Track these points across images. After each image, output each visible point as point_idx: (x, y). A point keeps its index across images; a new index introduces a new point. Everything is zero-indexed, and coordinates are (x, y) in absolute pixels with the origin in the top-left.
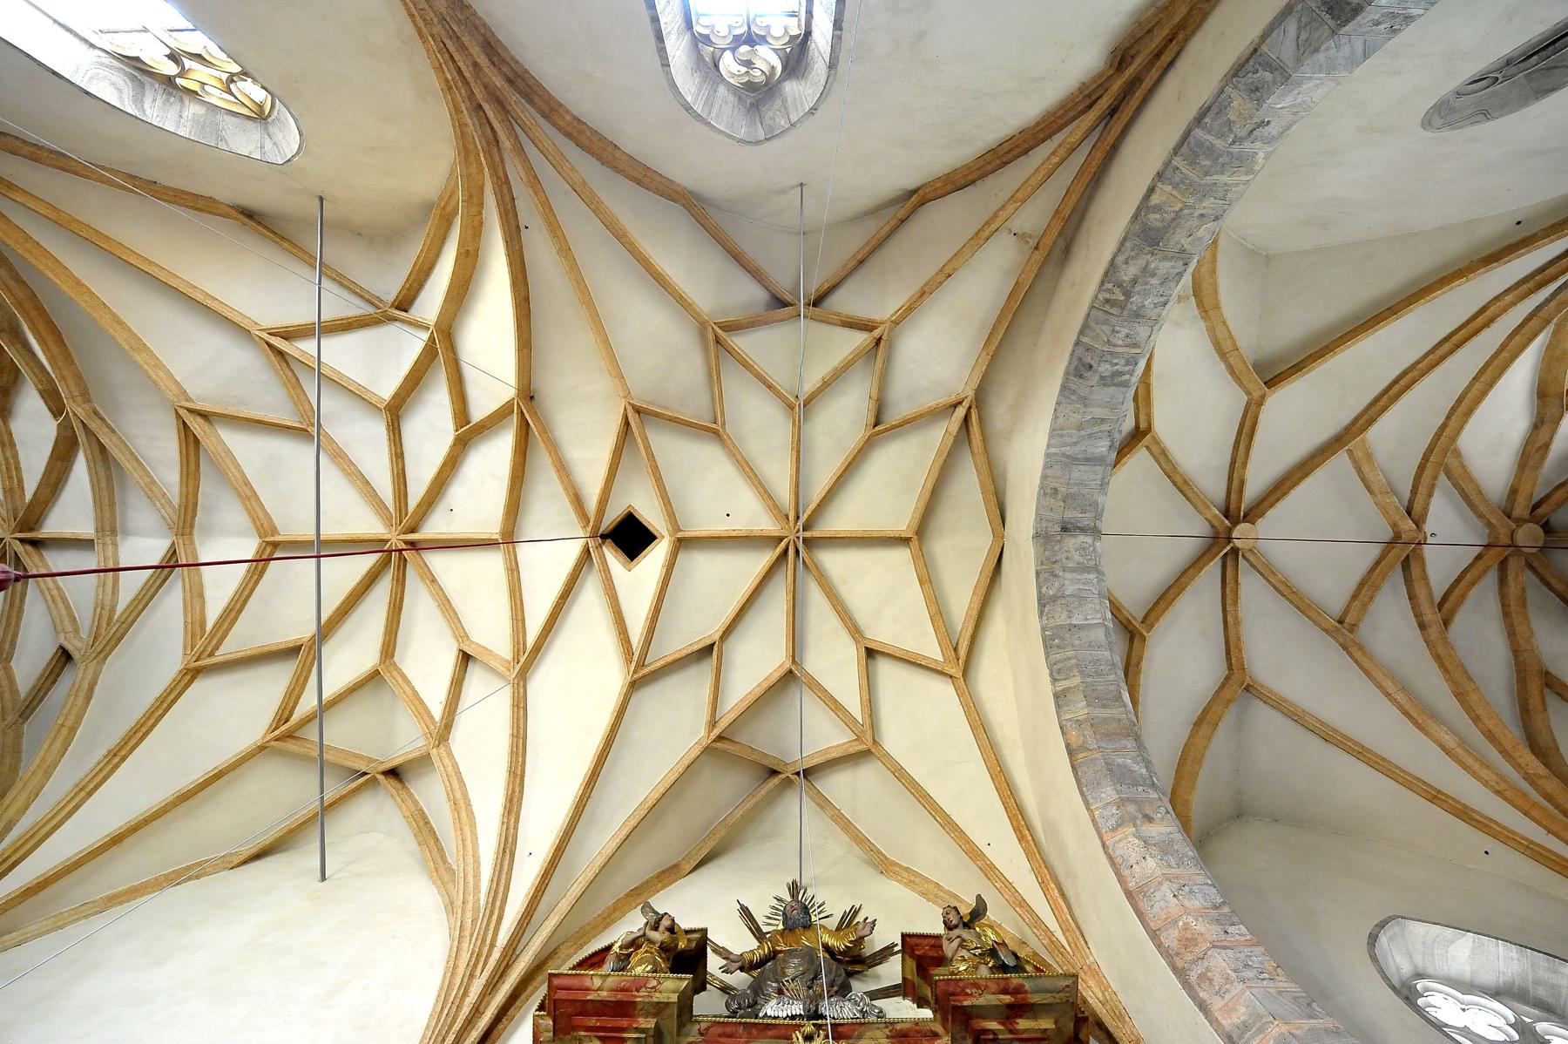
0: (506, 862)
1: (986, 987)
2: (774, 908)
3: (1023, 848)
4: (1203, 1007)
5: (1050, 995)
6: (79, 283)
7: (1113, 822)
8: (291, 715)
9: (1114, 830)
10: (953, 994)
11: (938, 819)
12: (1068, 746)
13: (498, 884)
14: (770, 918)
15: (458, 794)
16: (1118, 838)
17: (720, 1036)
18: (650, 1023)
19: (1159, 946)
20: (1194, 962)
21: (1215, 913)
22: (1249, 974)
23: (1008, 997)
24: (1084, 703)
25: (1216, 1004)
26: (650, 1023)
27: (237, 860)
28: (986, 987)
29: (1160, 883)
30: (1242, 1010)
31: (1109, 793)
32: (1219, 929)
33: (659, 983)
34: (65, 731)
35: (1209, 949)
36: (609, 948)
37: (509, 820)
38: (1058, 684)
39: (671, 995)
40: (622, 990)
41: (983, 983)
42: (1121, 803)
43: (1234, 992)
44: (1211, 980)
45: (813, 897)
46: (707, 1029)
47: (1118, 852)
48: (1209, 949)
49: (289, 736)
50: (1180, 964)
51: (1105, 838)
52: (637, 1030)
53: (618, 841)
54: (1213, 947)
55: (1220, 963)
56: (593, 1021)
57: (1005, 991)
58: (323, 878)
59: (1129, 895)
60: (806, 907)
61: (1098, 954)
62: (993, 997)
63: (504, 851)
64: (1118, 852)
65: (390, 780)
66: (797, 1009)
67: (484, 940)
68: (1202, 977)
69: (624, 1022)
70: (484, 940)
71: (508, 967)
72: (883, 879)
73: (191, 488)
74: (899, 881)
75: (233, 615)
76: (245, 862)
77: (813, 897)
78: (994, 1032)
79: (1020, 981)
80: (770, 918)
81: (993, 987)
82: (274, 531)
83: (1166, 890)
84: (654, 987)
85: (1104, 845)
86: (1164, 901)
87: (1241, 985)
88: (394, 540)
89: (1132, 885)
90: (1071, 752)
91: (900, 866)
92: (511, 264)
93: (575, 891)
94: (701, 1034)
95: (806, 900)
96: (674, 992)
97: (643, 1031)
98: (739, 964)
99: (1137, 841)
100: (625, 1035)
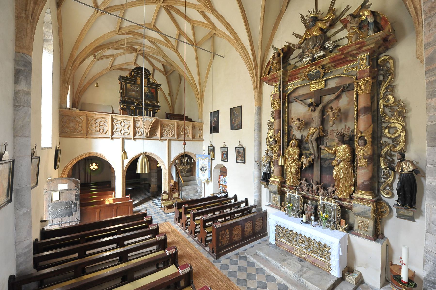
0: (245, 50)
5: (373, 40)
6: (90, 45)
8: (192, 42)
13: (246, 56)
15: (227, 38)
27: (212, 60)
34: (178, 67)
36: (270, 60)
37: (238, 43)
40: (273, 76)
44: (430, 25)
49: (196, 44)
53: (261, 27)
58: (224, 57)
63: (242, 49)
65: (257, 184)
67: (251, 66)
70: (251, 66)
71: (257, 67)
73: (136, 34)
75: (167, 40)
76: (213, 60)
79: (363, 40)
82: (150, 24)
88: (161, 5)
92: (228, 253)
93: (260, 47)
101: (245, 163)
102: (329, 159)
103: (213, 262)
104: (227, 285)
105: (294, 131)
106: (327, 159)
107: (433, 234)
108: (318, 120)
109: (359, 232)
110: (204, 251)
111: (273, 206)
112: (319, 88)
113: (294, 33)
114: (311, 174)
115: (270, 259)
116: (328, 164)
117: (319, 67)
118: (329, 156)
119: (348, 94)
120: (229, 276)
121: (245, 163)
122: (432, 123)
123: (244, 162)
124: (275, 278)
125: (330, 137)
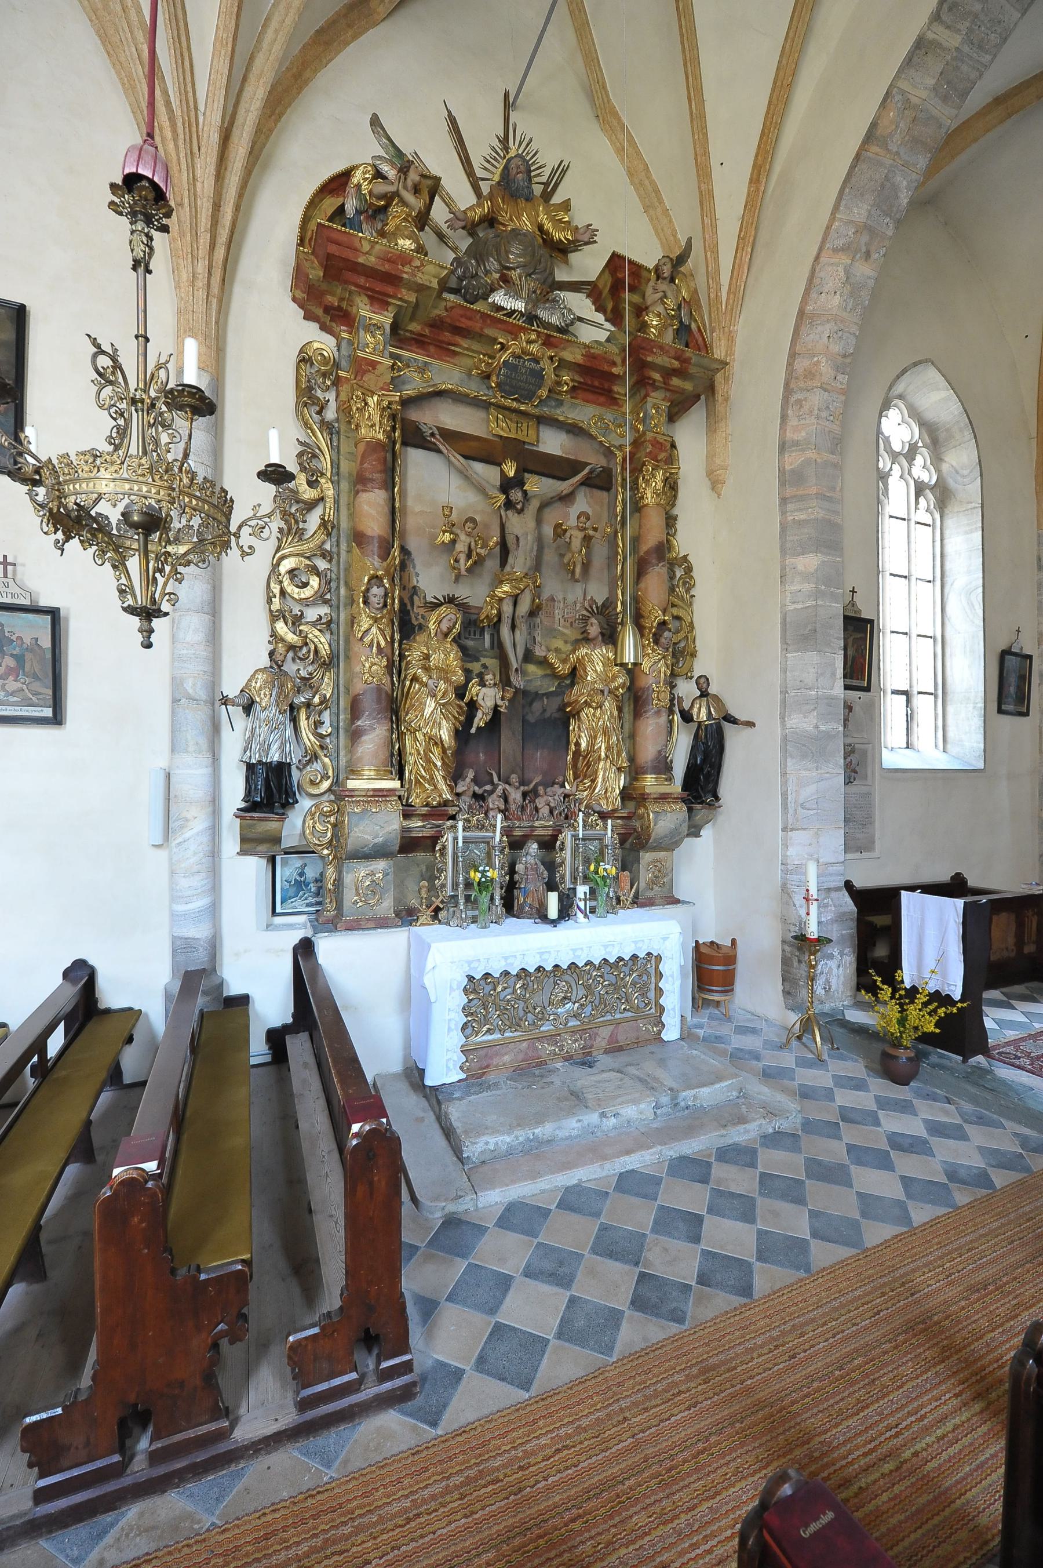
1: (667, 351)
2: (493, 149)
3: (749, 190)
4: (784, 418)
7: (840, 242)
9: (836, 250)
10: (643, 348)
11: (693, 107)
12: (874, 125)
14: (488, 161)
16: (832, 261)
17: (462, 316)
18: (412, 297)
19: (790, 364)
20: (801, 390)
21: (840, 359)
22: (824, 414)
23: (676, 363)
24: (933, 82)
25: (793, 422)
26: (412, 297)
28: (667, 351)
29: (828, 321)
30: (803, 434)
31: (860, 212)
32: (832, 373)
33: (422, 265)
35: (817, 387)
38: (940, 29)
39: (432, 279)
40: (389, 260)
41: (667, 348)
42: (865, 228)
43: (807, 422)
44: (801, 407)
45: (531, 140)
46: (452, 308)
47: (822, 274)
48: (817, 387)
50: (792, 385)
51: (823, 254)
52: (400, 299)
54: (821, 387)
55: (816, 399)
56: (362, 280)
57: (677, 358)
59: (801, 313)
60: (529, 166)
61: (742, 328)
62: (668, 359)
64: (822, 274)
66: (520, 305)
68: (799, 402)
69: (390, 290)
72: (595, 126)
74: (610, 140)
77: (531, 140)
78: (654, 381)
80: (488, 161)
81: (672, 353)
83: (827, 329)
84: (417, 267)
85: (817, 258)
86: (819, 336)
87: (815, 421)
89: (809, 308)
90: (870, 137)
91: (619, 119)
94: (446, 310)
95: (528, 154)
96: (435, 277)
97: (405, 301)
98: (463, 224)
99: (842, 274)
100: (390, 300)
101: (57, 719)
102: (543, 695)
103: (434, 1424)
104: (689, 1378)
105: (417, 575)
106: (536, 693)
107: (805, 829)
108: (532, 550)
109: (650, 894)
110: (239, 1475)
111: (357, 921)
112: (520, 436)
113: (416, 153)
114: (485, 754)
115: (545, 1130)
116: (541, 710)
117: (551, 358)
118: (541, 686)
119: (591, 497)
120: (609, 1349)
121: (57, 719)
122: (800, 606)
123: (48, 712)
124: (633, 1170)
125: (546, 622)
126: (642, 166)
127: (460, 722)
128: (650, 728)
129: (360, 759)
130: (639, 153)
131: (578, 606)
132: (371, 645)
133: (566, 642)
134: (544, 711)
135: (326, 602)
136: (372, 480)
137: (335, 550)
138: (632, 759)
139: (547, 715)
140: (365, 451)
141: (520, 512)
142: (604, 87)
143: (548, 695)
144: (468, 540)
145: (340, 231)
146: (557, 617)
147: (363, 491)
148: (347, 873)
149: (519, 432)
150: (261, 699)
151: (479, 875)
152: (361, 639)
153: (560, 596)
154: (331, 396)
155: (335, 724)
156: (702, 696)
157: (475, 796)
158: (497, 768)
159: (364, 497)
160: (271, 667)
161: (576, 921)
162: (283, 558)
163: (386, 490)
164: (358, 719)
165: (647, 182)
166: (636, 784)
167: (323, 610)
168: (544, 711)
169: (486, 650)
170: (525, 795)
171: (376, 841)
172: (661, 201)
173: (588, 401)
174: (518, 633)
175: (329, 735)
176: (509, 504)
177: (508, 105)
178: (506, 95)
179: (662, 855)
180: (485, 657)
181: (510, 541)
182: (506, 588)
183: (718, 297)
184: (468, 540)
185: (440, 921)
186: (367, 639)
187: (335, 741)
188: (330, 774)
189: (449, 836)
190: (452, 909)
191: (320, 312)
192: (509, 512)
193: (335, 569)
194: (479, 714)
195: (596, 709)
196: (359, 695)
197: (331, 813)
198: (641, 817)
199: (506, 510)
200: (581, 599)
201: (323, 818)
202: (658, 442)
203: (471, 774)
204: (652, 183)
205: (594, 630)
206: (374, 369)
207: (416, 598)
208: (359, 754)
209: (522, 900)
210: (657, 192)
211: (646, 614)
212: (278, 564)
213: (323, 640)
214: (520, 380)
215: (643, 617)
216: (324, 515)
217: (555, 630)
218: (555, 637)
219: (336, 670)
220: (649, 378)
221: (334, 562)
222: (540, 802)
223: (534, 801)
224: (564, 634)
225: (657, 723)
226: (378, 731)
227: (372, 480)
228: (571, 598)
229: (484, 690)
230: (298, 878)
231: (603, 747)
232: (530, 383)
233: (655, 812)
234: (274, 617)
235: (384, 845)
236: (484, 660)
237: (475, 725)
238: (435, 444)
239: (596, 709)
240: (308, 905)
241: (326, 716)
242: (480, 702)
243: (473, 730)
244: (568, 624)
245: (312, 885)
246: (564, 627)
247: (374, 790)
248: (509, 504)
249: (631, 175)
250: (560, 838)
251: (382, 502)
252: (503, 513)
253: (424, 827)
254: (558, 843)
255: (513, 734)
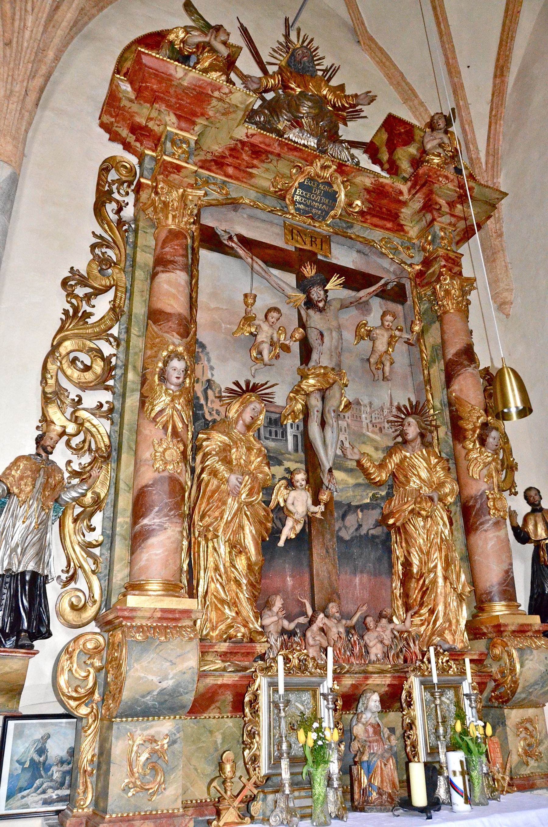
2: (281, 44)
3: (494, 85)
45: (312, 40)
77: (312, 40)
102: (357, 507)
105: (212, 368)
106: (349, 505)
114: (292, 576)
126: (398, 74)
127: (267, 530)
128: (491, 544)
129: (145, 568)
130: (394, 65)
131: (386, 411)
132: (165, 428)
133: (377, 449)
134: (360, 526)
135: (107, 388)
136: (172, 262)
137: (123, 336)
138: (473, 581)
139: (363, 531)
140: (167, 237)
141: (321, 310)
142: (363, 24)
143: (363, 507)
144: (270, 332)
145: (155, 57)
146: (365, 422)
147: (163, 272)
148: (117, 738)
149: (314, 245)
150: (21, 491)
151: (313, 736)
152: (154, 419)
153: (365, 400)
154: (131, 199)
155: (109, 532)
156: (534, 511)
157: (283, 631)
158: (308, 593)
159: (163, 277)
160: (38, 454)
161: (452, 810)
162: (65, 339)
163: (187, 273)
164: (144, 516)
165: (403, 84)
166: (484, 616)
167: (105, 397)
168: (360, 526)
169: (289, 453)
170: (348, 630)
171: (164, 684)
172: (416, 96)
173: (376, 226)
174: (328, 431)
175: (100, 545)
176: (310, 304)
177: (287, 26)
178: (287, 20)
179: (531, 712)
180: (289, 460)
181: (313, 337)
182: (312, 381)
183: (478, 159)
184: (270, 332)
185: (252, 818)
186: (163, 419)
187: (107, 554)
188: (97, 596)
189: (262, 681)
190: (270, 797)
191: (124, 132)
192: (311, 312)
193: (122, 356)
194: (289, 523)
195: (425, 518)
196: (146, 486)
197: (97, 650)
198: (497, 658)
199: (308, 308)
200: (388, 404)
201: (84, 658)
202: (450, 258)
203: (278, 603)
204: (407, 84)
205: (412, 431)
206: (179, 171)
207: (210, 392)
208: (142, 563)
209: (365, 780)
210: (413, 90)
211: (465, 415)
212: (59, 344)
213: (102, 430)
214: (314, 200)
215: (461, 418)
216: (114, 301)
217: (364, 435)
218: (364, 443)
219: (114, 465)
220: (436, 203)
221: (121, 348)
222: (371, 638)
223: (362, 637)
224: (373, 440)
225: (498, 537)
226: (169, 532)
227: (172, 262)
228: (377, 403)
229: (293, 494)
230: (36, 758)
231: (439, 567)
232: (323, 204)
233: (521, 650)
234: (46, 399)
235: (174, 693)
236: (287, 464)
237: (283, 538)
238: (232, 248)
239: (425, 518)
240: (46, 802)
241: (97, 520)
242: (291, 508)
243: (281, 543)
244: (377, 430)
245: (54, 769)
246: (373, 432)
247: (163, 610)
248: (310, 304)
249: (389, 78)
250: (406, 686)
251: (183, 283)
252: (303, 312)
253: (224, 669)
254: (404, 694)
255: (327, 552)
